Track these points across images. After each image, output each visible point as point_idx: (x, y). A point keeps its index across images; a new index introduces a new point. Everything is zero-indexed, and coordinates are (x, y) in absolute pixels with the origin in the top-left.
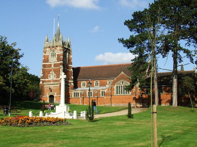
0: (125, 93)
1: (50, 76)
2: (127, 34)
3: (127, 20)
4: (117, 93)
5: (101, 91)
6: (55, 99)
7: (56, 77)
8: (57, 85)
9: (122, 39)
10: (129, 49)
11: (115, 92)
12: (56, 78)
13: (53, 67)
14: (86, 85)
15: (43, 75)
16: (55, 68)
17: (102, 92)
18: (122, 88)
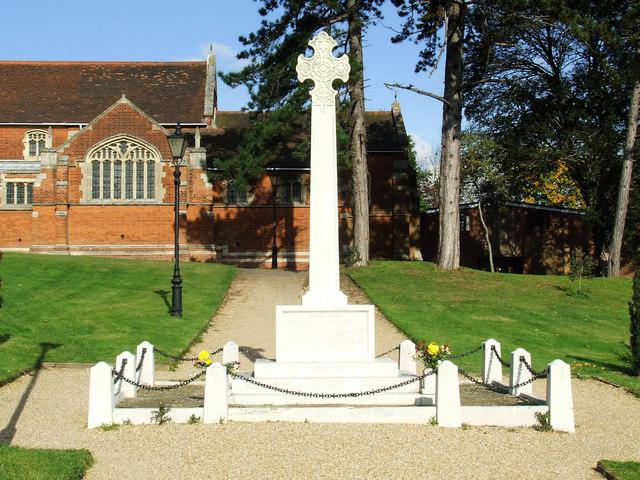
4: (96, 196)
11: (86, 187)
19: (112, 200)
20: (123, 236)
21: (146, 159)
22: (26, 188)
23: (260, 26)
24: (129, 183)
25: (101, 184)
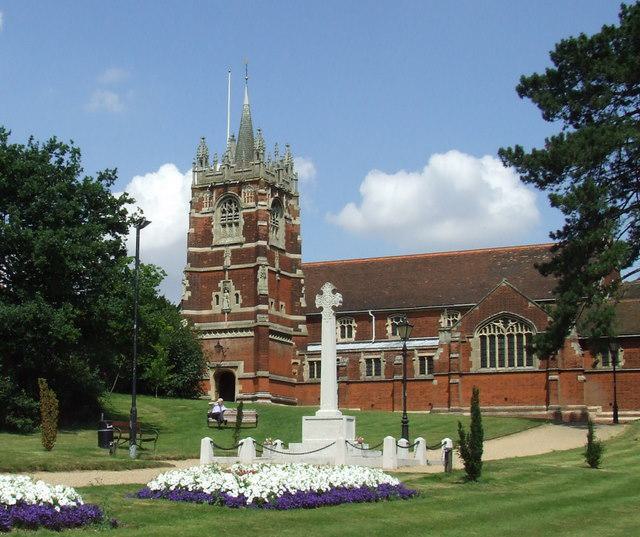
0: (525, 364)
1: (217, 296)
2: (537, 131)
3: (528, 75)
4: (484, 365)
5: (418, 354)
6: (238, 387)
7: (241, 301)
8: (244, 334)
9: (514, 151)
10: (547, 192)
11: (475, 357)
12: (242, 306)
13: (227, 262)
14: (354, 332)
15: (189, 293)
16: (237, 266)
17: (422, 359)
18: (501, 344)
19: (506, 369)
20: (506, 399)
21: (497, 333)
22: (516, 361)
23: (564, 223)
24: (511, 354)
25: (488, 355)
